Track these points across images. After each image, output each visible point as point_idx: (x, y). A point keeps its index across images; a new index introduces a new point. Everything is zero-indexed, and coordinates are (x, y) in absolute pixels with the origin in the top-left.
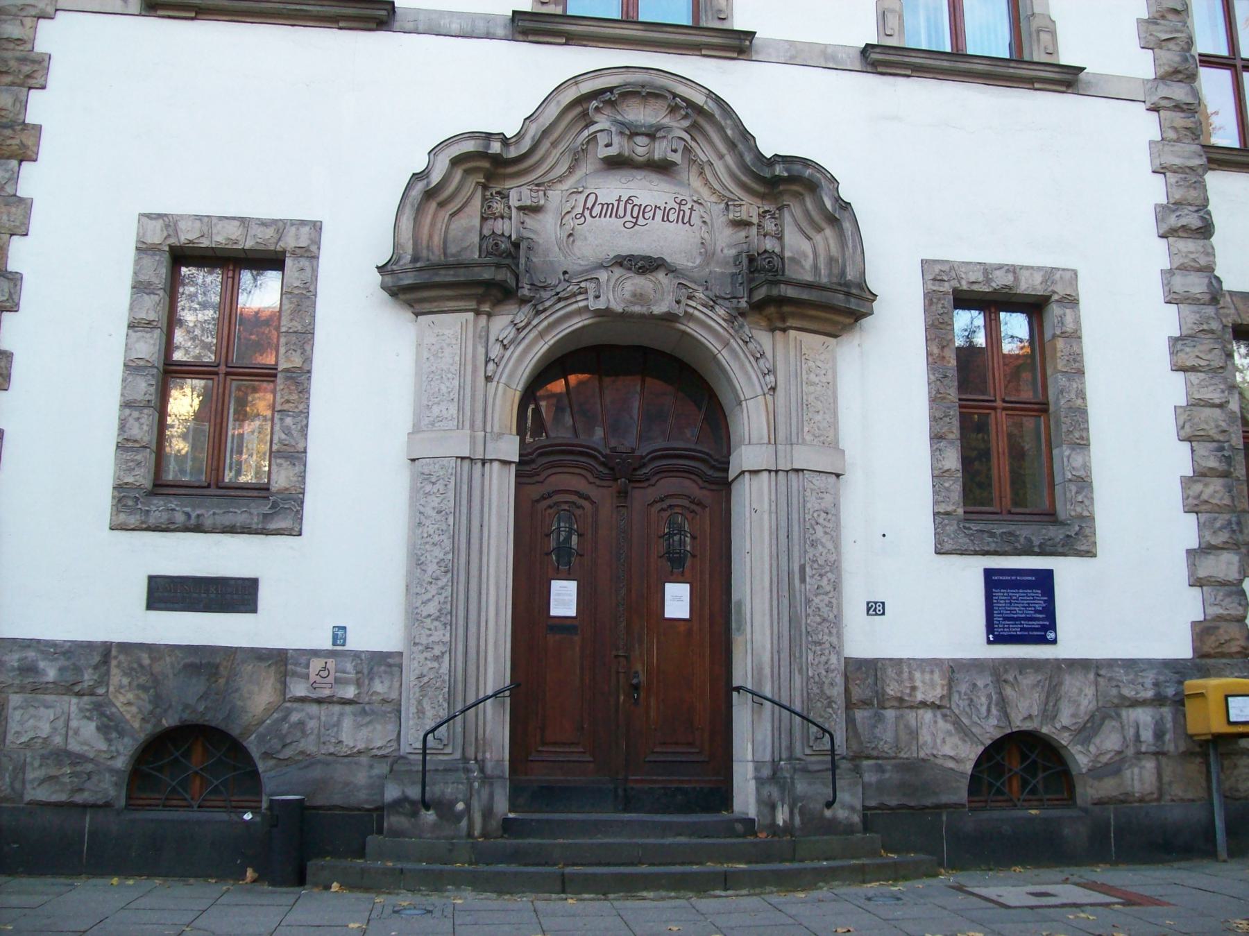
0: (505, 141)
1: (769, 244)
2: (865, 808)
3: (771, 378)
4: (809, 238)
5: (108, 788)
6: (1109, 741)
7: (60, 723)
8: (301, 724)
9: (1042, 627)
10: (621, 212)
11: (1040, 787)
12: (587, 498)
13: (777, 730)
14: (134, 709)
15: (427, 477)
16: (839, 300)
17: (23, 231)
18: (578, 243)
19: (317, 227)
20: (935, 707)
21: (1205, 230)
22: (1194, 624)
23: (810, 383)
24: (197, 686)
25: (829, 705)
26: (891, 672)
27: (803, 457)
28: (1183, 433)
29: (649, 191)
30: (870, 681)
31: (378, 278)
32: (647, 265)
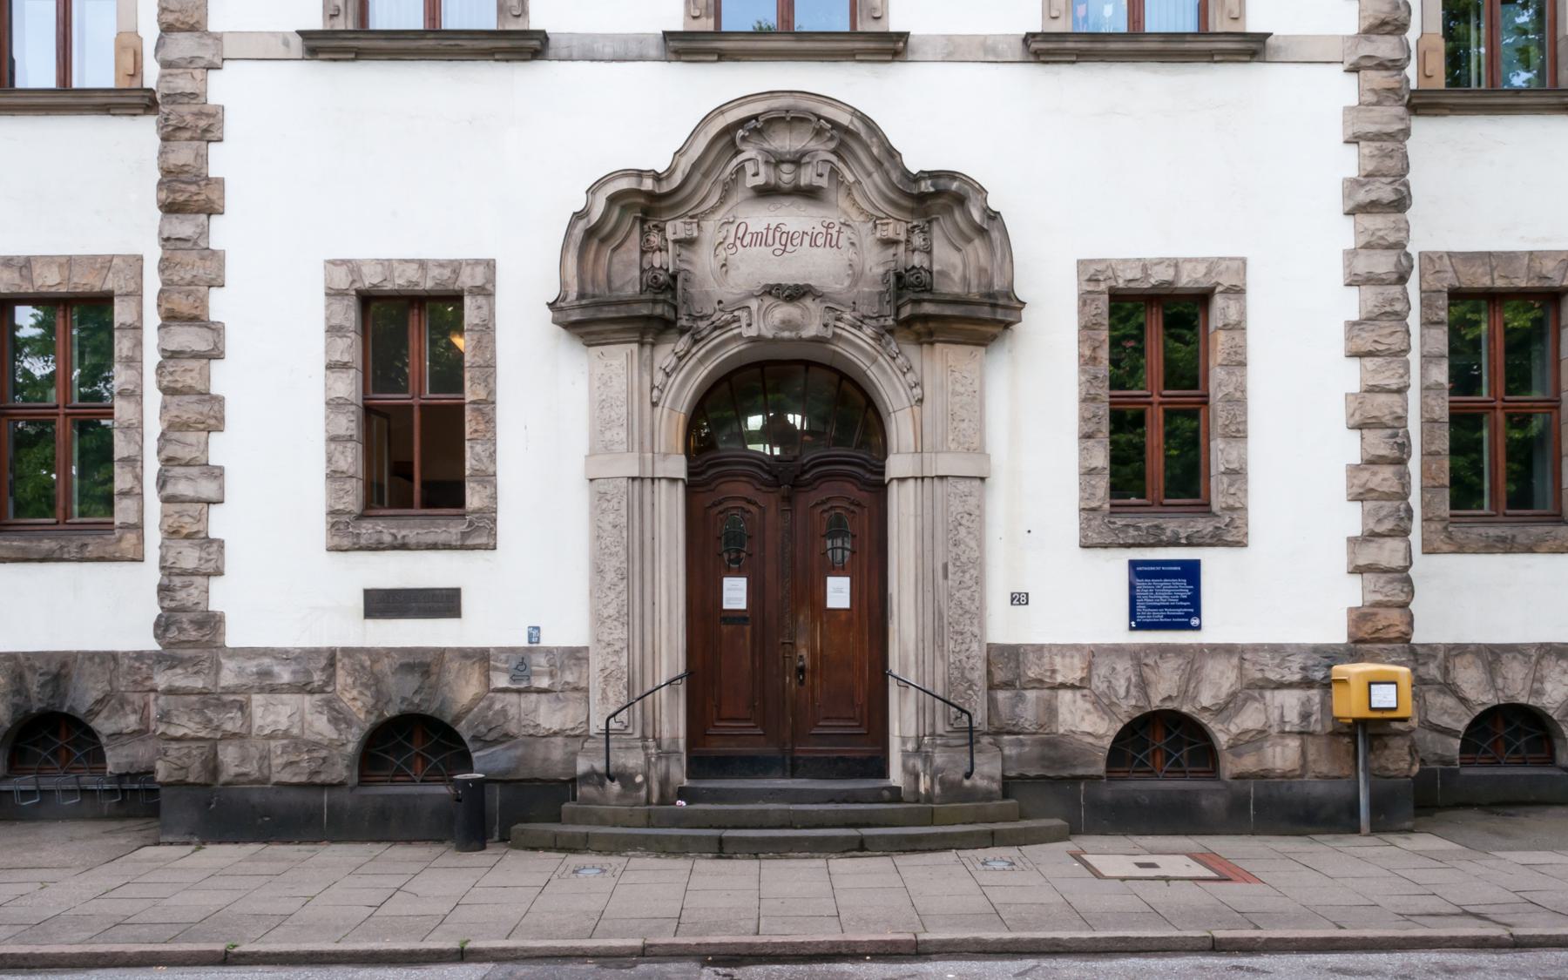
0: (657, 177)
1: (918, 260)
2: (1004, 777)
3: (917, 391)
4: (959, 250)
5: (340, 771)
6: (1250, 719)
7: (296, 718)
8: (504, 711)
9: (1187, 613)
10: (770, 241)
11: (1184, 762)
12: (755, 503)
13: (921, 710)
14: (359, 704)
15: (602, 496)
16: (985, 312)
17: (217, 282)
18: (732, 273)
19: (490, 265)
20: (1073, 687)
21: (1400, 203)
22: (1351, 610)
23: (955, 394)
24: (413, 682)
25: (970, 688)
26: (1031, 656)
27: (944, 464)
28: (1352, 422)
29: (795, 218)
30: (1012, 664)
31: (549, 314)
32: (796, 294)
